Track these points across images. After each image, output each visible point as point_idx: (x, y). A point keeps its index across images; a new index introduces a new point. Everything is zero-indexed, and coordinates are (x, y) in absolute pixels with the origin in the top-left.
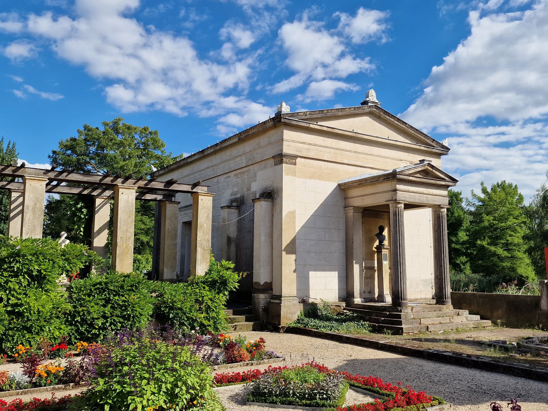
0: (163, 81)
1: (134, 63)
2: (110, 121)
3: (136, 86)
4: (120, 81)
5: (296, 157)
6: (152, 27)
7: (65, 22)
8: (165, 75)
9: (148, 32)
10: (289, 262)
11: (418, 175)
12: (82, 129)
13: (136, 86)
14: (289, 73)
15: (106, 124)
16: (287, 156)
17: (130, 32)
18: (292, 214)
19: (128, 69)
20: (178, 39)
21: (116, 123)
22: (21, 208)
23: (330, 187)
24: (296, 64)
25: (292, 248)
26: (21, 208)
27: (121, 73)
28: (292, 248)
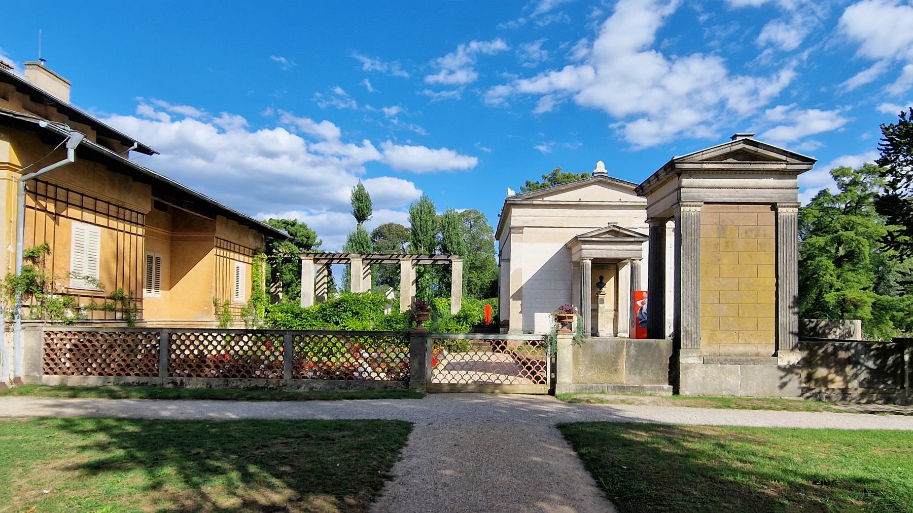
0: (689, 106)
1: (657, 93)
2: (548, 174)
3: (661, 116)
4: (643, 115)
5: (523, 227)
6: (674, 57)
7: (587, 72)
8: (691, 98)
9: (669, 59)
10: (515, 307)
11: (607, 236)
12: (524, 186)
13: (661, 116)
14: (867, 63)
15: (545, 178)
16: (514, 228)
17: (652, 63)
18: (519, 271)
19: (652, 101)
20: (707, 59)
21: (554, 174)
22: (317, 286)
23: (558, 246)
24: (873, 50)
25: (518, 296)
26: (317, 286)
27: (644, 106)
28: (518, 296)
